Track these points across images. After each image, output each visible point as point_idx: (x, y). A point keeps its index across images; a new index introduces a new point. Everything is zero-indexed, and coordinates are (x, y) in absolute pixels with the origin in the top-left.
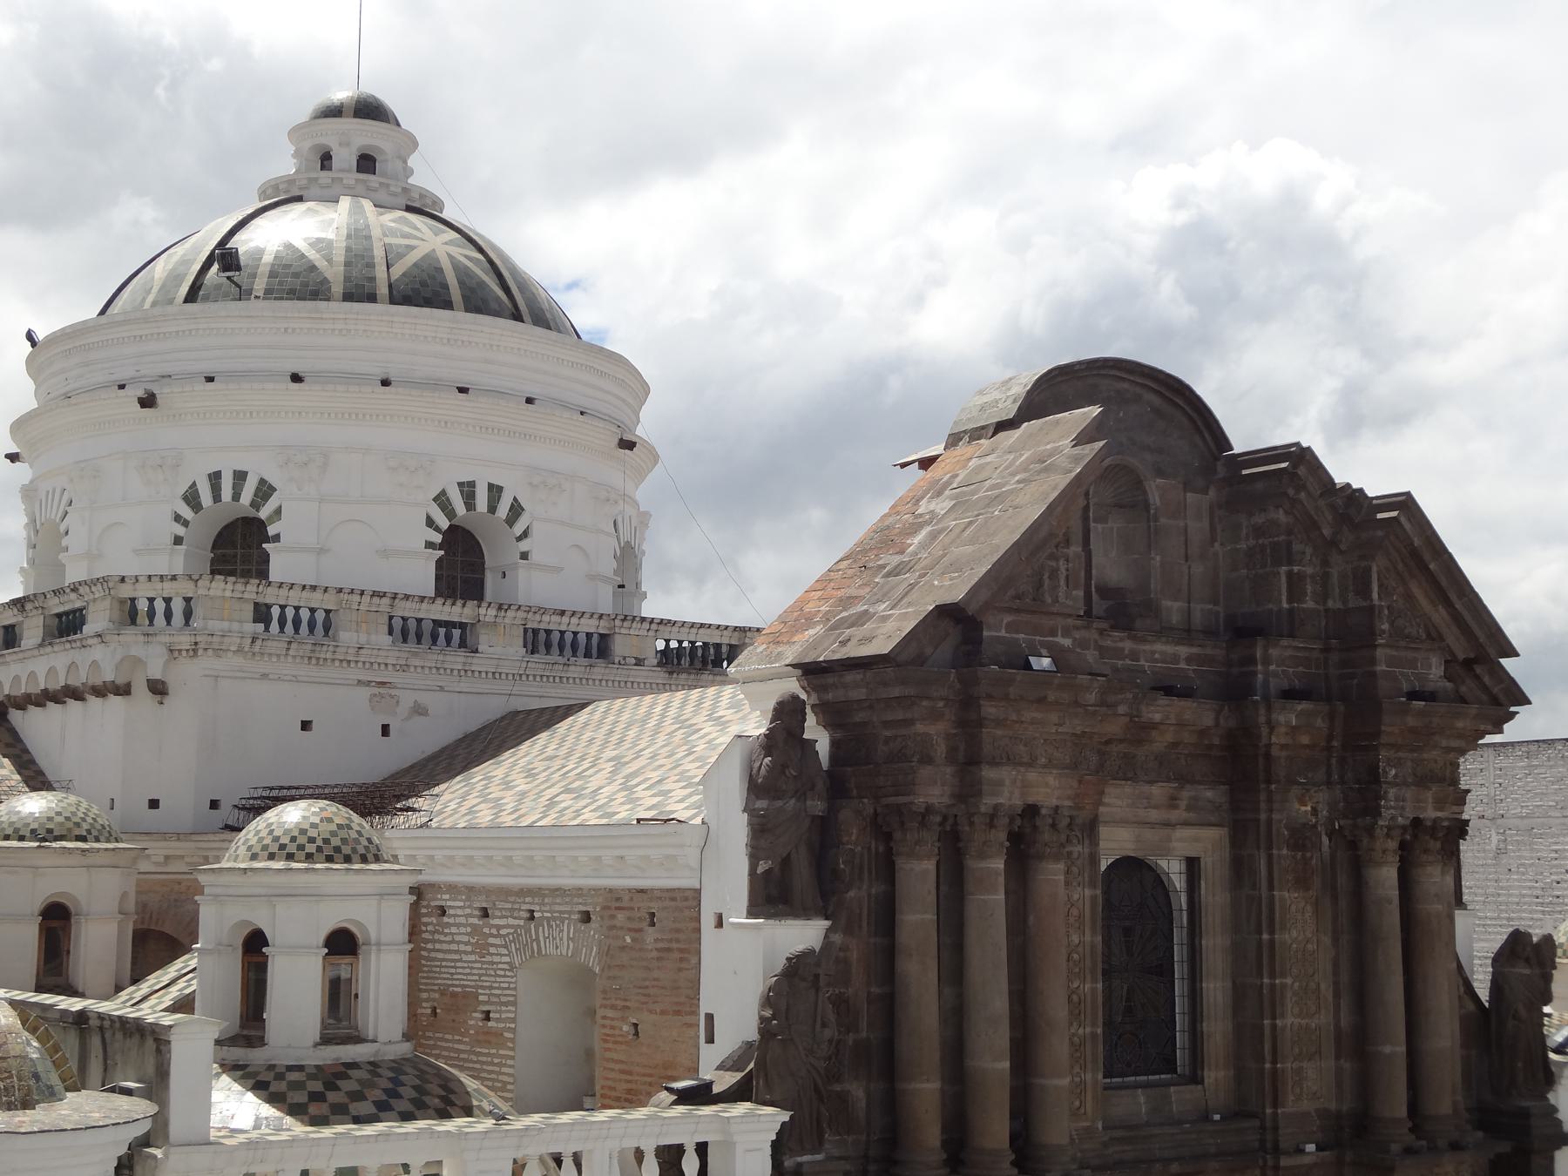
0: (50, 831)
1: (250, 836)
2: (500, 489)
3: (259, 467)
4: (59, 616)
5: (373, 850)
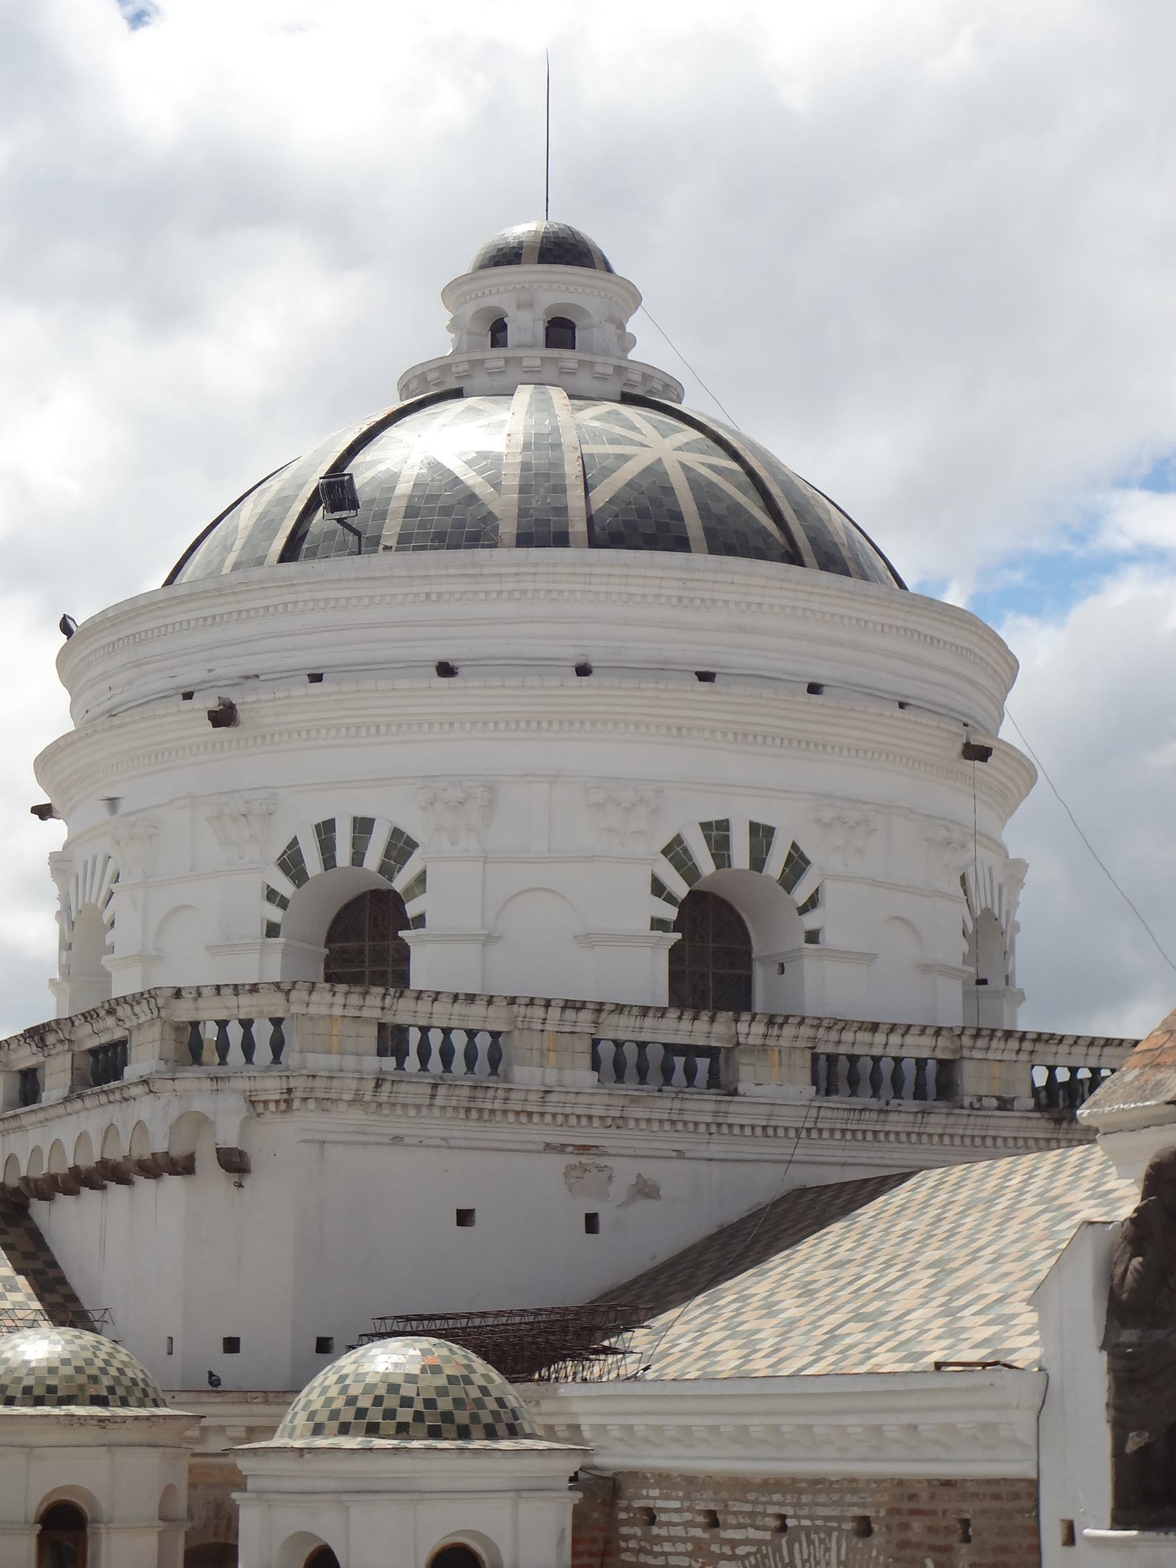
0: (52, 1389)
1: (314, 1396)
2: (769, 831)
3: (391, 811)
4: (94, 1052)
5: (506, 1417)
